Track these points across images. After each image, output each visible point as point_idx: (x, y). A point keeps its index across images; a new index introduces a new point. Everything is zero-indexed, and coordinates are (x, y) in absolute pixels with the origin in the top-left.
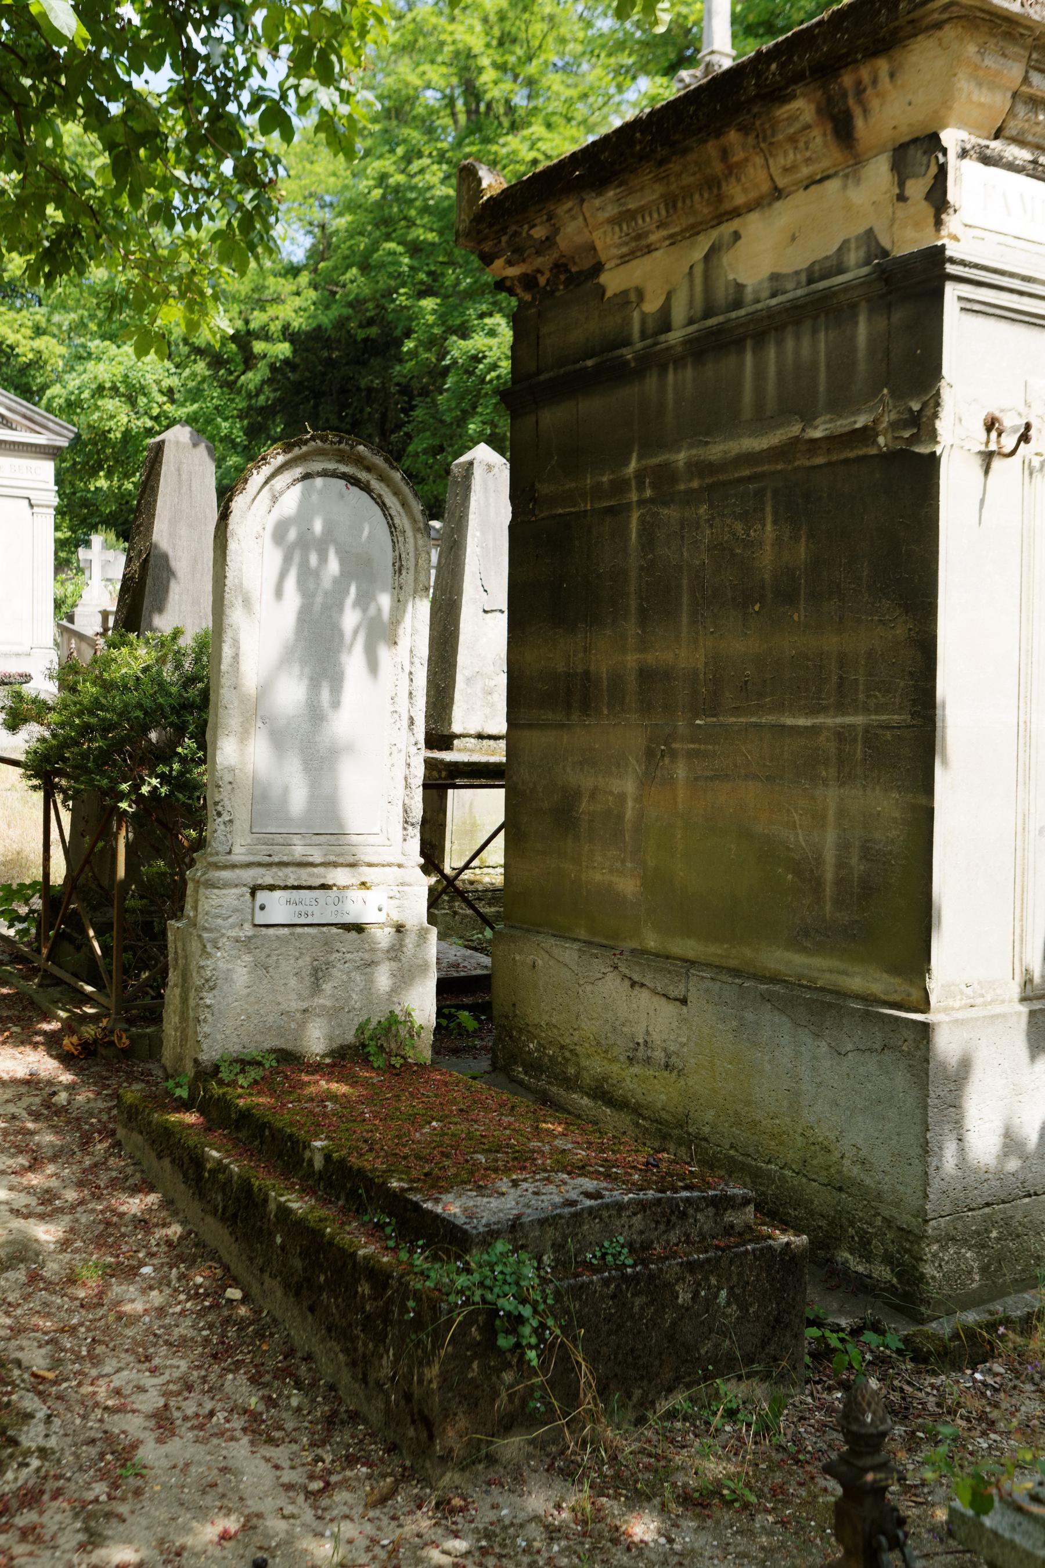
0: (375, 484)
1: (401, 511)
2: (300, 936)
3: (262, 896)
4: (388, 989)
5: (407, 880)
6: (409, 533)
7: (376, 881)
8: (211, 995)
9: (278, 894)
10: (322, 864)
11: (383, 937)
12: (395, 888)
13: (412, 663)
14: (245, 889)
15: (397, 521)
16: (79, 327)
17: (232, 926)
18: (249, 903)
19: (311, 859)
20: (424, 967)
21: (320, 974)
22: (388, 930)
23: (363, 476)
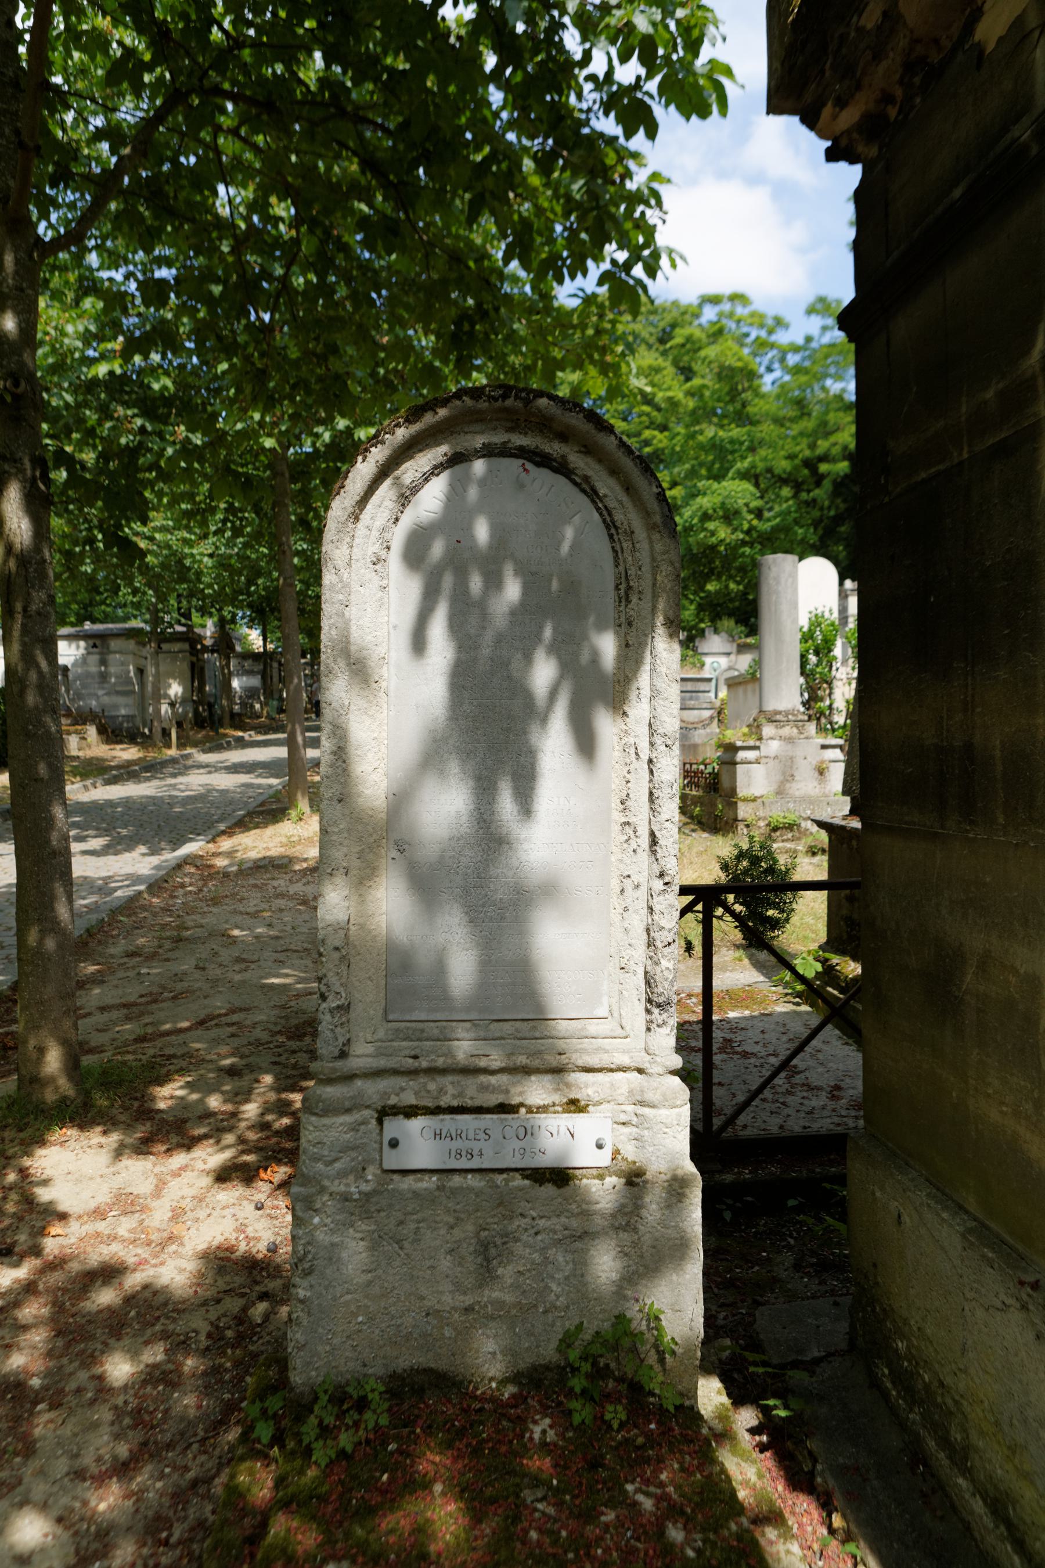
0: (577, 461)
1: (625, 499)
2: (454, 1192)
3: (394, 1127)
4: (614, 1276)
5: (650, 1096)
6: (641, 534)
7: (596, 1098)
8: (305, 1283)
9: (417, 1123)
10: (501, 1071)
11: (603, 1192)
12: (630, 1108)
13: (652, 744)
14: (367, 1113)
15: (618, 517)
16: (693, 474)
17: (342, 1174)
18: (375, 1135)
19: (483, 1063)
20: (679, 1249)
21: (493, 1252)
22: (611, 1180)
23: (555, 448)
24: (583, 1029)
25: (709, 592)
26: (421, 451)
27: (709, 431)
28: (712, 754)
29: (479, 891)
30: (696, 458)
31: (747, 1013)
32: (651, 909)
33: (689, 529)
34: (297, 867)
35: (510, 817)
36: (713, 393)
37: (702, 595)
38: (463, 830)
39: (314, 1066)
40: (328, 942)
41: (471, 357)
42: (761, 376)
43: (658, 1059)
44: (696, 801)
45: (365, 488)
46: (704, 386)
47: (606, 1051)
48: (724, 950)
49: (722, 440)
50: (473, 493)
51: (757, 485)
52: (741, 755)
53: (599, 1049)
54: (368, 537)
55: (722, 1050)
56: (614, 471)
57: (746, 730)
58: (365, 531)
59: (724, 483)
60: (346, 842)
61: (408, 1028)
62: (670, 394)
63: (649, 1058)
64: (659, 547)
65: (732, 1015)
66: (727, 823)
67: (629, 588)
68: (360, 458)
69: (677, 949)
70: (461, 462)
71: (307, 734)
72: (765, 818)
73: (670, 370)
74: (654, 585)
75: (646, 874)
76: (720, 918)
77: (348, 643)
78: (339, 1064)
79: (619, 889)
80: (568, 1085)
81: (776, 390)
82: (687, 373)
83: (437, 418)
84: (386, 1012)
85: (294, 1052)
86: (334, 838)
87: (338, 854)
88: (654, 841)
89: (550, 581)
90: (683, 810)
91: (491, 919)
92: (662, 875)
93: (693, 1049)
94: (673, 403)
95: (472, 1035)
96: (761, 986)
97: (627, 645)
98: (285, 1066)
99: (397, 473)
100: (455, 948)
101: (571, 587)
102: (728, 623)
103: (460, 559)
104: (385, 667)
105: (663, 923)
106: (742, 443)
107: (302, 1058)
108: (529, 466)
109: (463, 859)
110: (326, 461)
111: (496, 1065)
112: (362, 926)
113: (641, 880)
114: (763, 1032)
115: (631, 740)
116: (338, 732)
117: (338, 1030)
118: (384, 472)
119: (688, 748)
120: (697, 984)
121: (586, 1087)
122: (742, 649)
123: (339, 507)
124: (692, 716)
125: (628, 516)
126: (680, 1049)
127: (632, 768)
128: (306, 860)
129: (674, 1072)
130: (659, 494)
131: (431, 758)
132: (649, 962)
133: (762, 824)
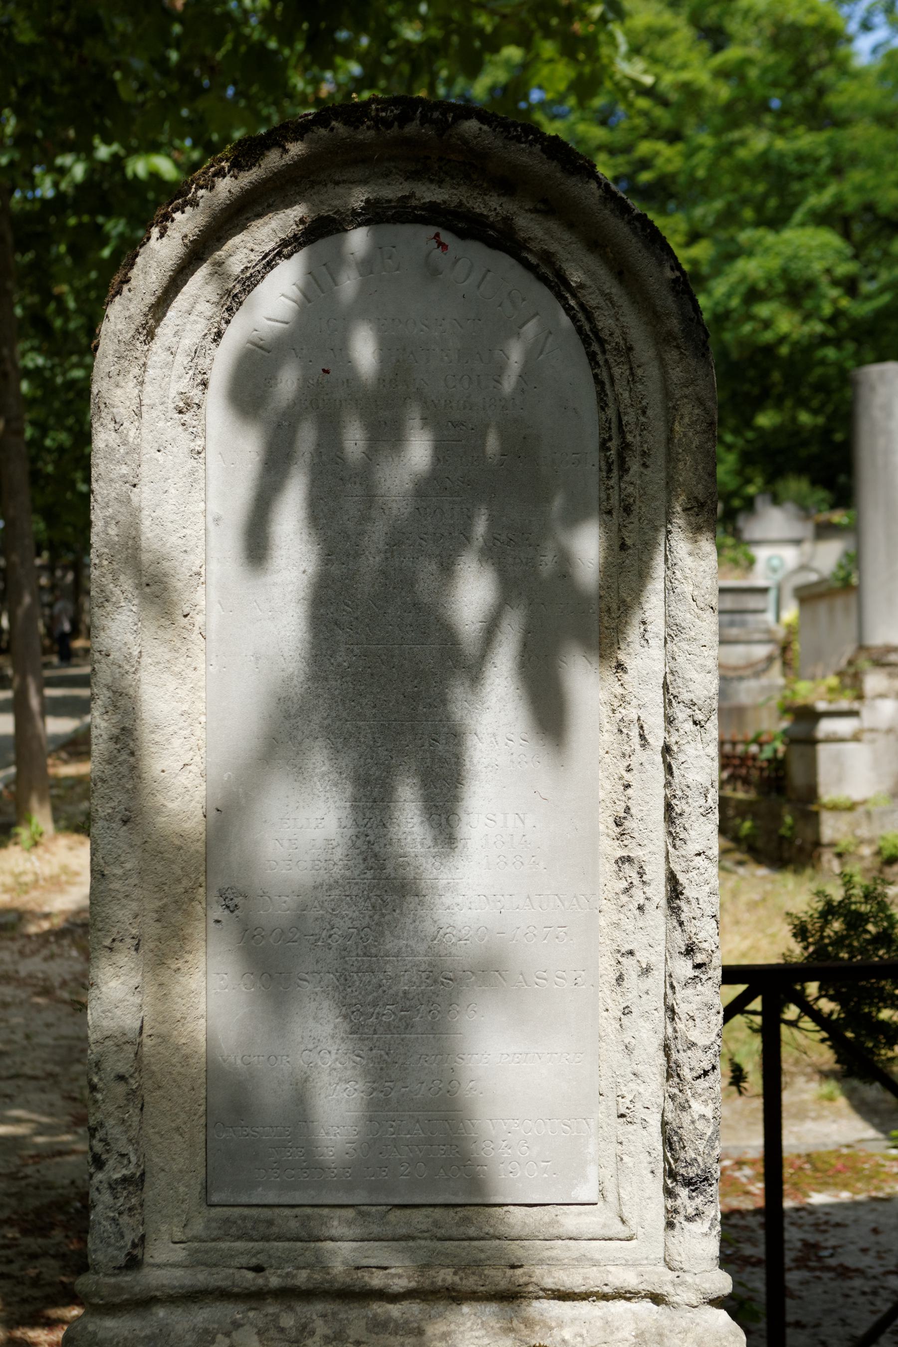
0: (529, 225)
6: (644, 351)
10: (193, 1297)
13: (669, 720)
15: (605, 322)
16: (729, 217)
19: (377, 1280)
23: (491, 206)
24: (553, 1223)
25: (760, 430)
26: (259, 216)
27: (758, 141)
28: (774, 725)
29: (366, 978)
30: (735, 190)
31: (845, 1196)
32: (671, 1011)
33: (723, 317)
34: (32, 929)
35: (419, 849)
36: (765, 70)
37: (750, 435)
38: (337, 871)
39: (84, 1283)
40: (107, 1066)
41: (332, 30)
42: (850, 40)
43: (688, 1278)
44: (744, 810)
45: (165, 282)
46: (747, 61)
47: (595, 1264)
48: (800, 1081)
49: (782, 155)
50: (349, 284)
51: (846, 235)
52: (826, 727)
53: (581, 1260)
54: (169, 365)
55: (801, 1263)
56: (597, 243)
57: (833, 681)
58: (164, 356)
59: (788, 234)
60: (137, 893)
61: (244, 1218)
62: (685, 76)
63: (672, 1275)
64: (676, 374)
65: (817, 1199)
66: (801, 849)
67: (625, 446)
68: (155, 232)
69: (720, 1080)
70: (329, 233)
71: (50, 692)
72: (870, 842)
73: (685, 33)
74: (670, 440)
75: (661, 949)
76: (793, 1024)
77: (137, 548)
78: (126, 1279)
79: (613, 976)
80: (529, 1323)
81: (878, 63)
82: (715, 37)
83: (287, 158)
84: (206, 1189)
85: (34, 1256)
86: (116, 885)
87: (122, 915)
88: (675, 890)
89: (483, 437)
90: (723, 830)
91: (389, 1028)
92: (689, 951)
93: (747, 1261)
94: (691, 94)
95: (357, 1231)
96: (872, 1148)
97: (623, 547)
98: (20, 1282)
99: (220, 254)
100: (325, 1078)
101: (522, 446)
102: (796, 485)
103: (328, 397)
104: (201, 590)
105: (694, 1035)
106: (817, 161)
107: (49, 1269)
108: (446, 237)
109: (337, 921)
110: (78, 213)
111: (400, 1284)
112: (164, 1039)
113: (653, 959)
114: (875, 1231)
115: (632, 713)
116: (121, 702)
117: (125, 1219)
118: (197, 253)
119: (730, 713)
120: (754, 1142)
121: (561, 1325)
122: (824, 531)
123: (120, 317)
124: (737, 654)
125: (623, 321)
126: (726, 1261)
127: (634, 761)
128: (47, 916)
129: (717, 1302)
130: (676, 281)
131: (280, 741)
132: (670, 1106)
133: (866, 851)
